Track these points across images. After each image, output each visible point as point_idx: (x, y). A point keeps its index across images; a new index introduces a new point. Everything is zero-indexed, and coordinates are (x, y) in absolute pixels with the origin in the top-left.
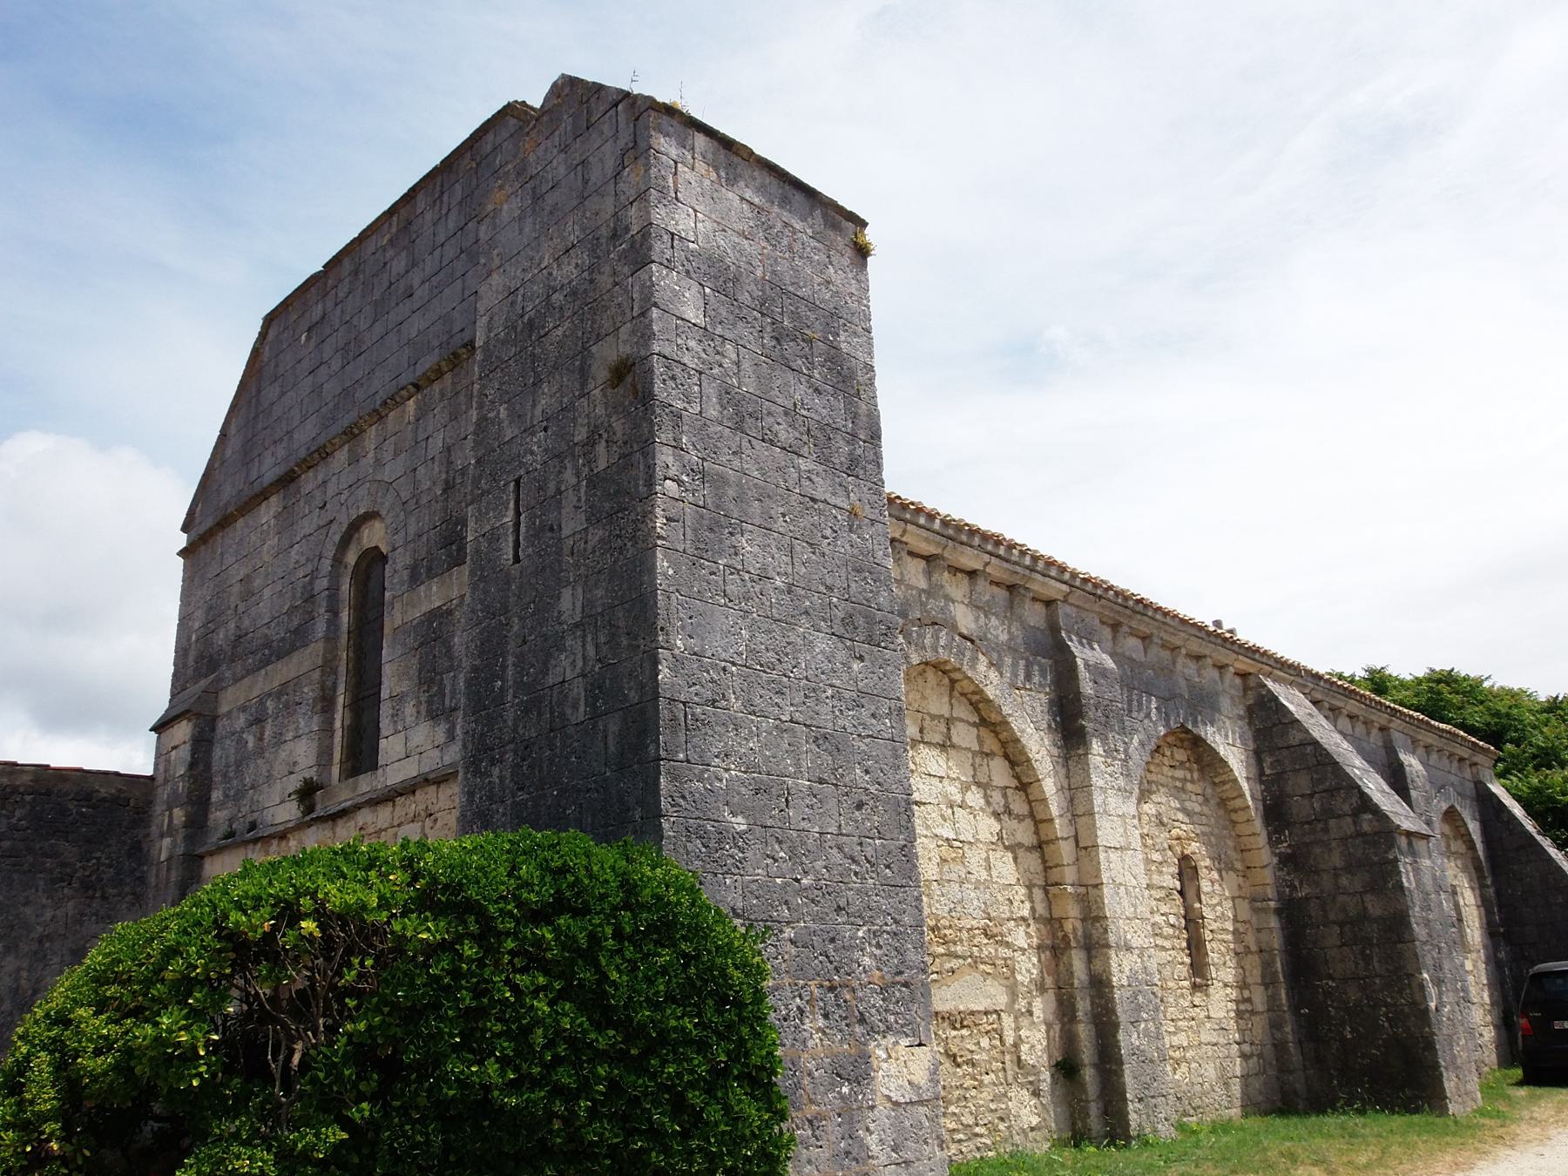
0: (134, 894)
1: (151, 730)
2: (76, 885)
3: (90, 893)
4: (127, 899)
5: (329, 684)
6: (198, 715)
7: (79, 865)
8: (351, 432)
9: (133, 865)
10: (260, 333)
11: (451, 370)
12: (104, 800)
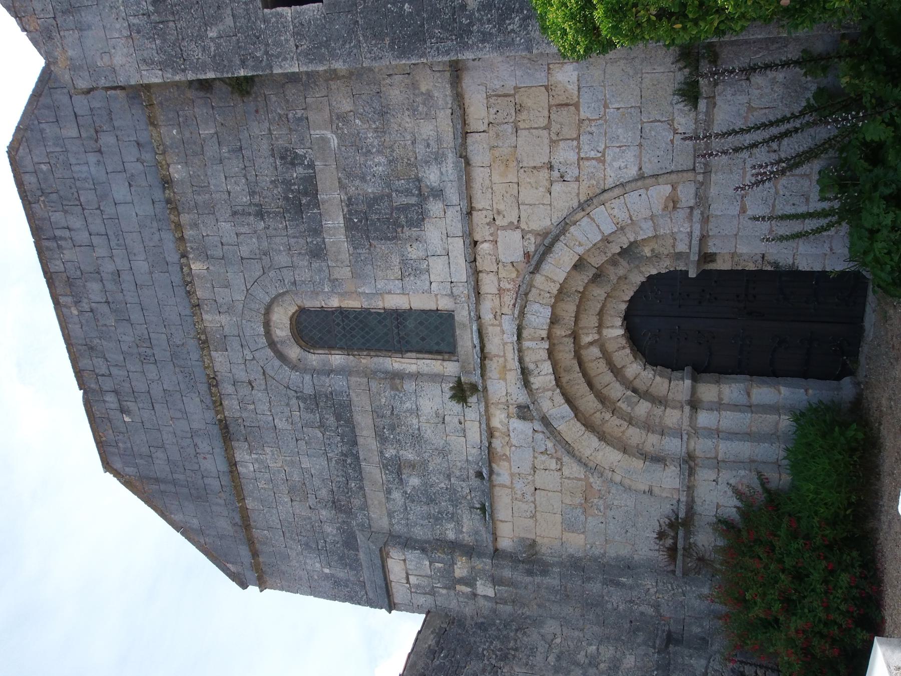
0: (517, 630)
1: (390, 613)
2: (502, 664)
3: (510, 656)
4: (520, 636)
5: (382, 376)
6: (385, 544)
7: (486, 662)
8: (204, 343)
9: (494, 628)
10: (115, 476)
11: (179, 214)
12: (438, 643)
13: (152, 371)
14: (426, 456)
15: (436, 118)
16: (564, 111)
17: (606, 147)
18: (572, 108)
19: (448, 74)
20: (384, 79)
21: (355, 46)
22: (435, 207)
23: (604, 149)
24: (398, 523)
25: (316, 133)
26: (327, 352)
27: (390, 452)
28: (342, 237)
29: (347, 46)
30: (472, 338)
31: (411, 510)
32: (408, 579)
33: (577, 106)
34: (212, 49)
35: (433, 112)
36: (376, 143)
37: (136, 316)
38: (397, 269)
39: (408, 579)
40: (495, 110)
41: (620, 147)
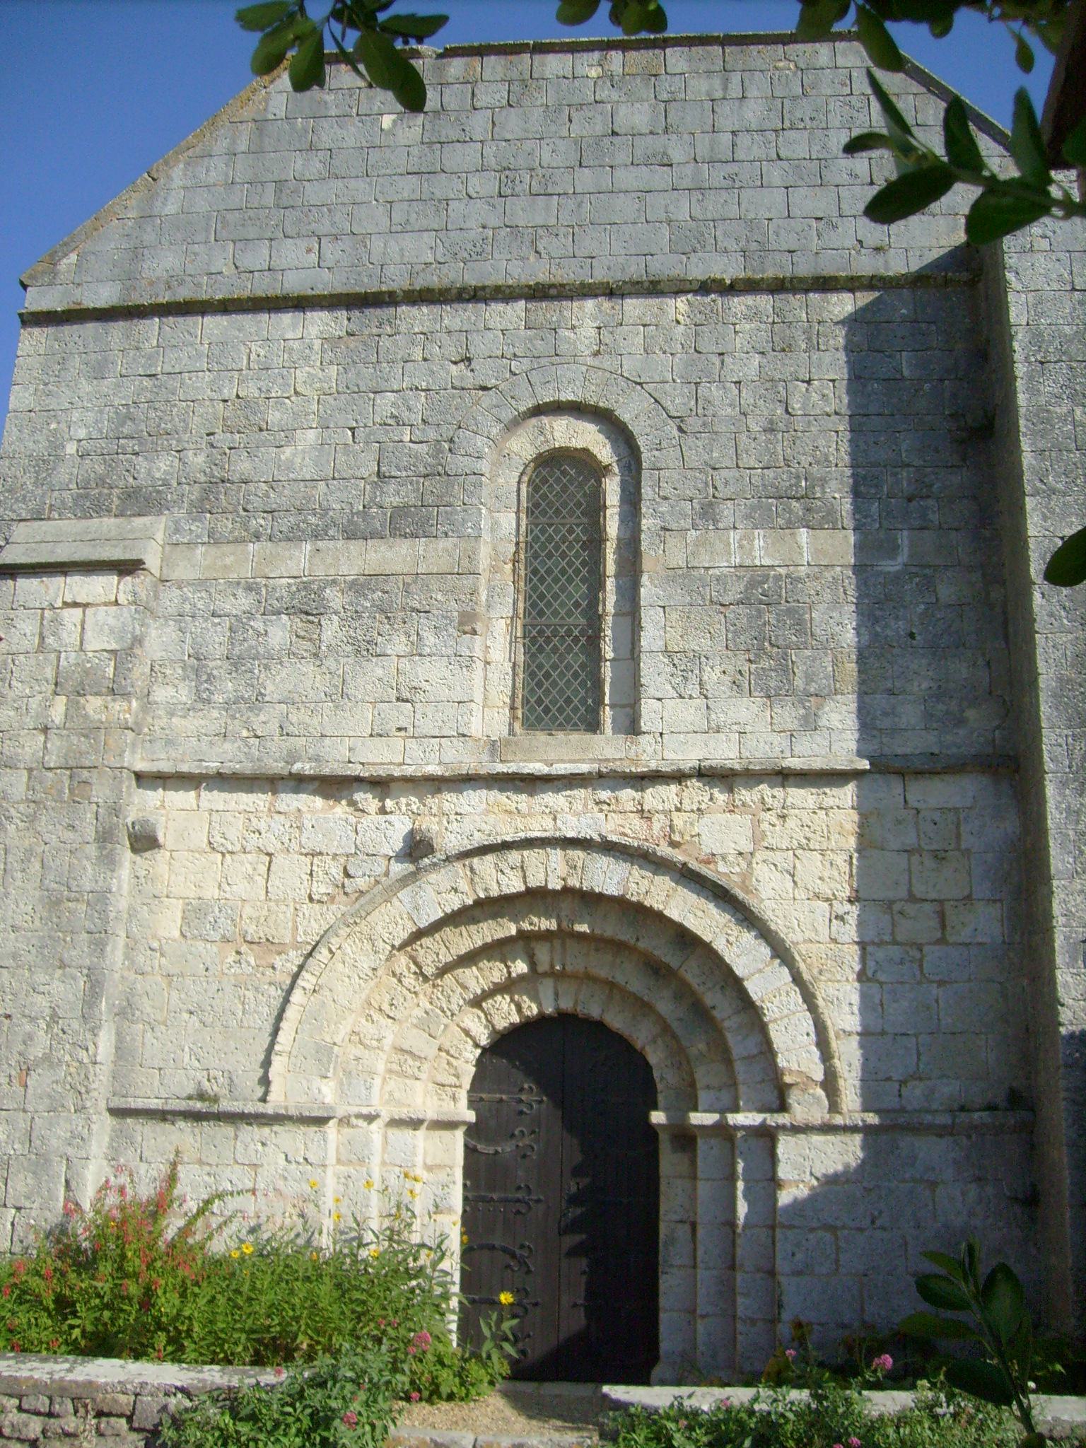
13: (483, 185)
14: (330, 663)
15: (926, 729)
16: (934, 923)
17: (881, 984)
18: (939, 935)
19: (990, 750)
20: (983, 654)
21: (1062, 624)
22: (788, 715)
23: (877, 981)
24: (185, 599)
25: (904, 538)
26: (524, 504)
27: (335, 599)
28: (738, 560)
29: (1063, 613)
30: (563, 761)
31: (215, 625)
32: (75, 605)
33: (942, 941)
34: (1058, 410)
35: (935, 725)
36: (889, 632)
37: (586, 178)
38: (682, 645)
39: (75, 605)
40: (937, 819)
41: (882, 1005)
